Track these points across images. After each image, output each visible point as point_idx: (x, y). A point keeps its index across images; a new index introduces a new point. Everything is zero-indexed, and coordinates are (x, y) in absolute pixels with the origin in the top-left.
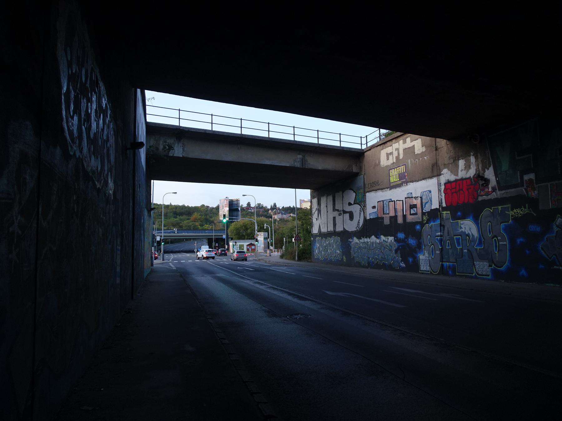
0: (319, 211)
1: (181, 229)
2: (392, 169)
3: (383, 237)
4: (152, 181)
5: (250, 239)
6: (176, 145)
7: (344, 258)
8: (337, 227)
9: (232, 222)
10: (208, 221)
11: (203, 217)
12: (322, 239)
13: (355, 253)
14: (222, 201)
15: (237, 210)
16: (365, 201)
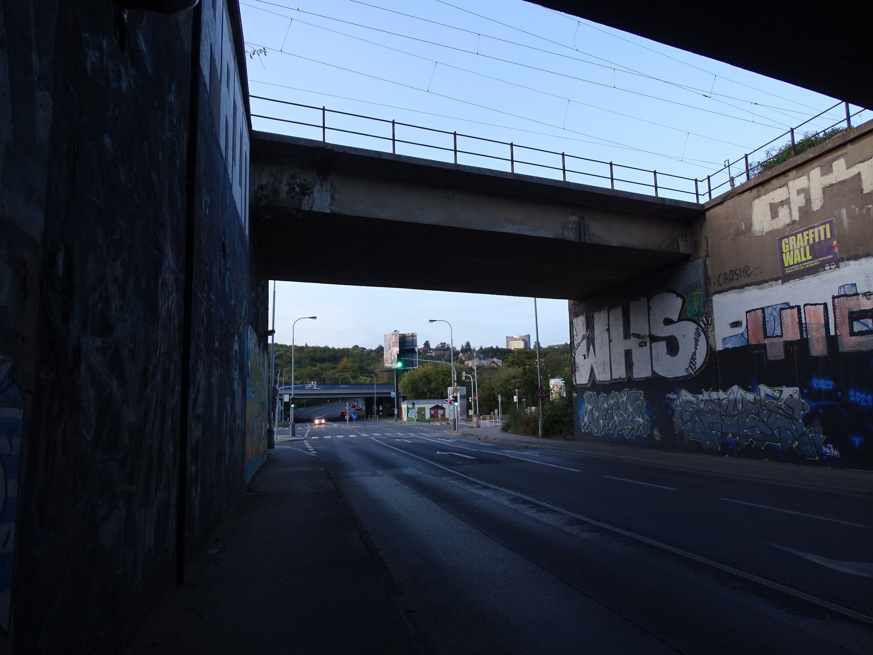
0: (590, 340)
1: (321, 382)
2: (787, 237)
3: (764, 389)
4: (271, 282)
5: (434, 398)
6: (317, 187)
7: (656, 432)
8: (635, 370)
9: (407, 370)
10: (363, 371)
11: (357, 364)
12: (598, 394)
13: (684, 424)
14: (388, 337)
15: (412, 351)
16: (709, 313)
